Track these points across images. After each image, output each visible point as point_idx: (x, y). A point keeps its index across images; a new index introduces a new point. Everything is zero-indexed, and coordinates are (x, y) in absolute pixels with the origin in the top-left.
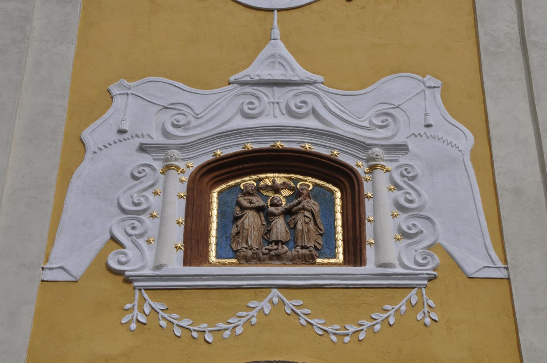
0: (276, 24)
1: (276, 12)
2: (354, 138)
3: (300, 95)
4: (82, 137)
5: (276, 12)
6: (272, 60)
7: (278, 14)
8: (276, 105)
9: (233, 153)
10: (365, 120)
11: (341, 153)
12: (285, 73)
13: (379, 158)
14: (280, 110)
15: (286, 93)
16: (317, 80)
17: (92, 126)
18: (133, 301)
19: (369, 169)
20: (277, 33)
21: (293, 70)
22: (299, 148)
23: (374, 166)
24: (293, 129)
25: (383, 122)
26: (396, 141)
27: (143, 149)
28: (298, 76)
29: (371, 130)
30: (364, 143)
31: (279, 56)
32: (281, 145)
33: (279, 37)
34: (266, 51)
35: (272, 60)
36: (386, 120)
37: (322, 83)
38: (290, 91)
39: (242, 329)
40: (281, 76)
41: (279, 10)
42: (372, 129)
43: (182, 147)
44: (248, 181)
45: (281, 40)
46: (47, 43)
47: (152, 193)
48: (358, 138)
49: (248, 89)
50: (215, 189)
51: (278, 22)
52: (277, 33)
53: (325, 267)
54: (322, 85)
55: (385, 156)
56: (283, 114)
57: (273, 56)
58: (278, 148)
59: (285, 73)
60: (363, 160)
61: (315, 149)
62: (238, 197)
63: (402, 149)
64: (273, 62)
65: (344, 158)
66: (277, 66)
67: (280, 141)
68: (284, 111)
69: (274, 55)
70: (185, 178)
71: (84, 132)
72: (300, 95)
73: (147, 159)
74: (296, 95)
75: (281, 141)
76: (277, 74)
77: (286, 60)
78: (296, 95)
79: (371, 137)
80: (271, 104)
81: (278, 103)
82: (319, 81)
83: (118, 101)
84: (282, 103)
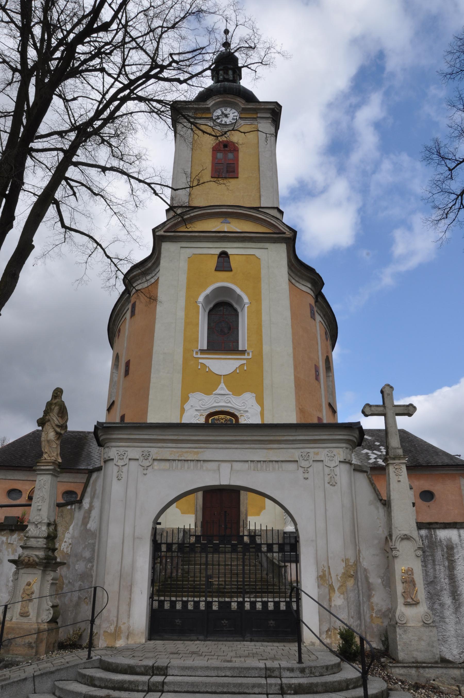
9: (146, 621)
17: (186, 404)
18: (96, 539)
20: (222, 381)
26: (246, 410)
27: (196, 410)
34: (220, 387)
39: (60, 48)
43: (204, 410)
44: (216, 417)
47: (129, 360)
49: (217, 396)
52: (222, 381)
62: (35, 636)
63: (247, 411)
70: (204, 417)
73: (197, 413)
76: (222, 392)
83: (190, 398)
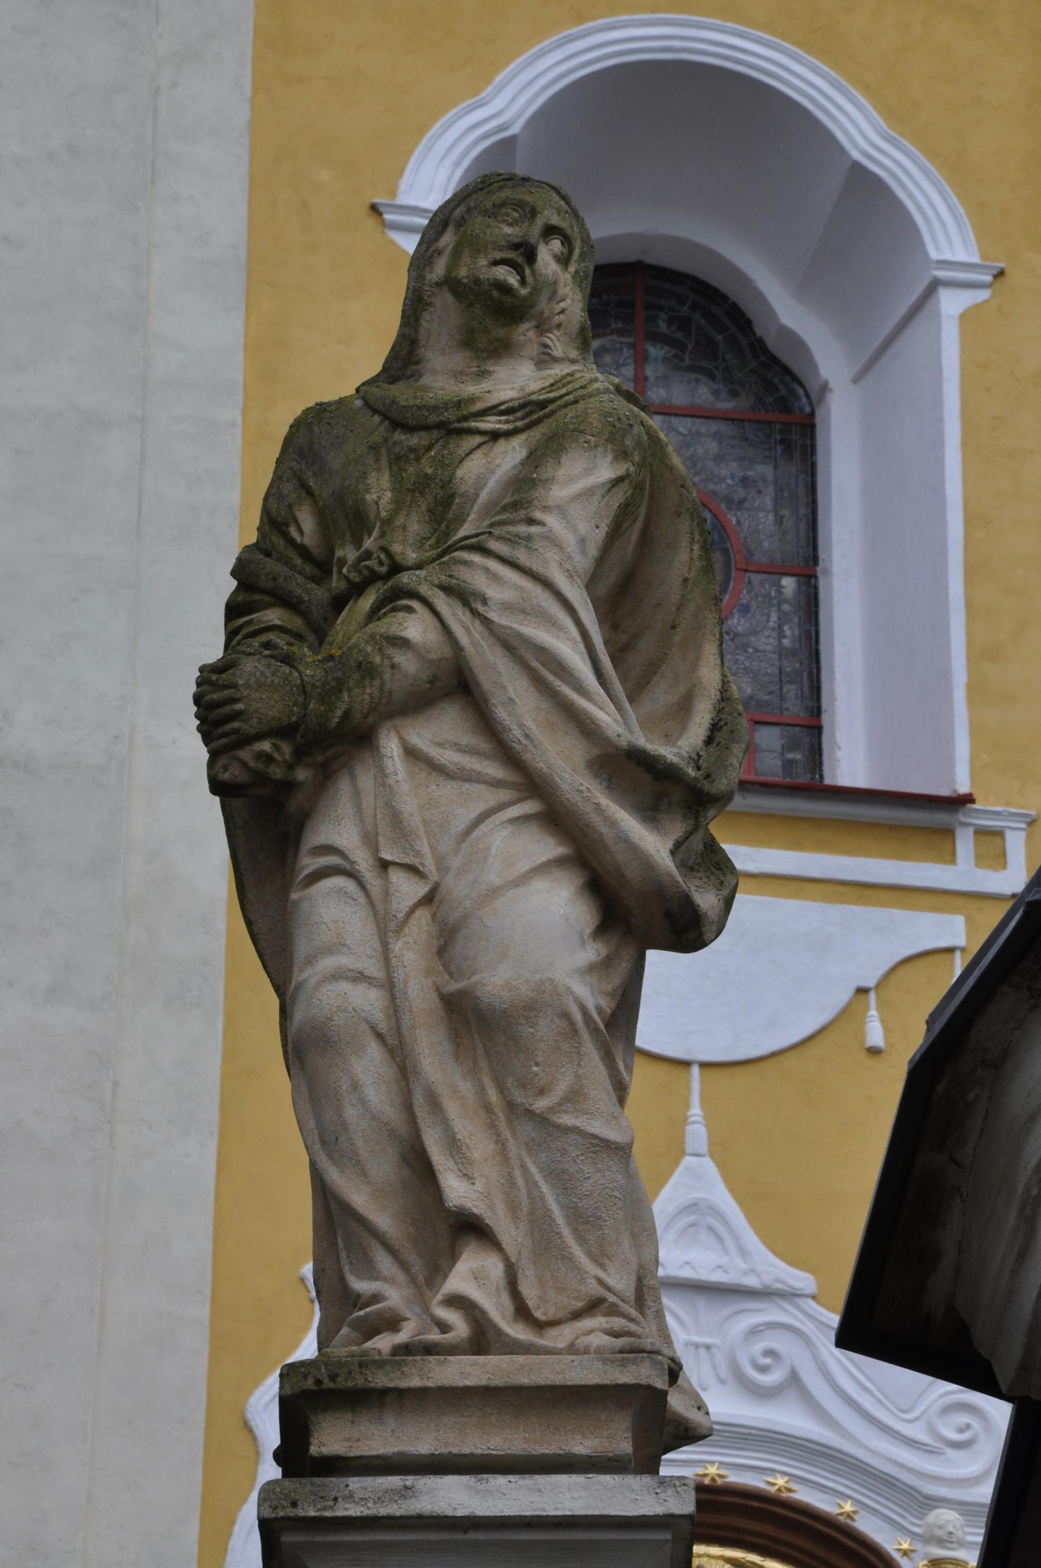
0: (696, 1110)
1: (695, 1070)
2: (894, 1474)
3: (761, 1331)
4: (249, 1416)
5: (695, 1070)
6: (692, 1218)
7: (702, 1081)
8: (702, 1351)
10: (917, 1419)
11: (861, 1511)
12: (723, 1261)
13: (955, 1539)
14: (715, 1368)
15: (728, 1318)
16: (801, 1290)
19: (929, 1564)
20: (697, 1134)
21: (743, 1252)
22: (762, 1485)
23: (942, 1561)
24: (750, 1434)
25: (961, 1430)
28: (757, 1275)
29: (933, 1452)
30: (918, 1492)
31: (710, 1208)
32: (720, 1476)
33: (704, 1149)
35: (692, 1218)
36: (968, 1426)
37: (814, 1297)
38: (737, 1313)
40: (715, 1270)
41: (704, 1065)
42: (934, 1450)
45: (712, 1155)
46: (150, 1128)
48: (905, 1477)
50: (376, 600)
51: (704, 1101)
52: (697, 1134)
53: (827, 572)
54: (812, 1303)
55: (967, 1529)
56: (723, 1382)
57: (692, 1207)
58: (712, 1483)
59: (723, 1261)
60: (914, 1537)
61: (803, 1495)
64: (694, 1225)
65: (868, 1527)
66: (704, 1236)
67: (717, 1464)
68: (724, 1372)
69: (695, 1204)
71: (253, 1400)
72: (761, 1331)
74: (754, 1332)
75: (721, 1463)
77: (726, 1223)
78: (755, 1330)
79: (933, 1474)
80: (692, 1349)
81: (708, 1347)
82: (807, 1292)
84: (718, 1348)
